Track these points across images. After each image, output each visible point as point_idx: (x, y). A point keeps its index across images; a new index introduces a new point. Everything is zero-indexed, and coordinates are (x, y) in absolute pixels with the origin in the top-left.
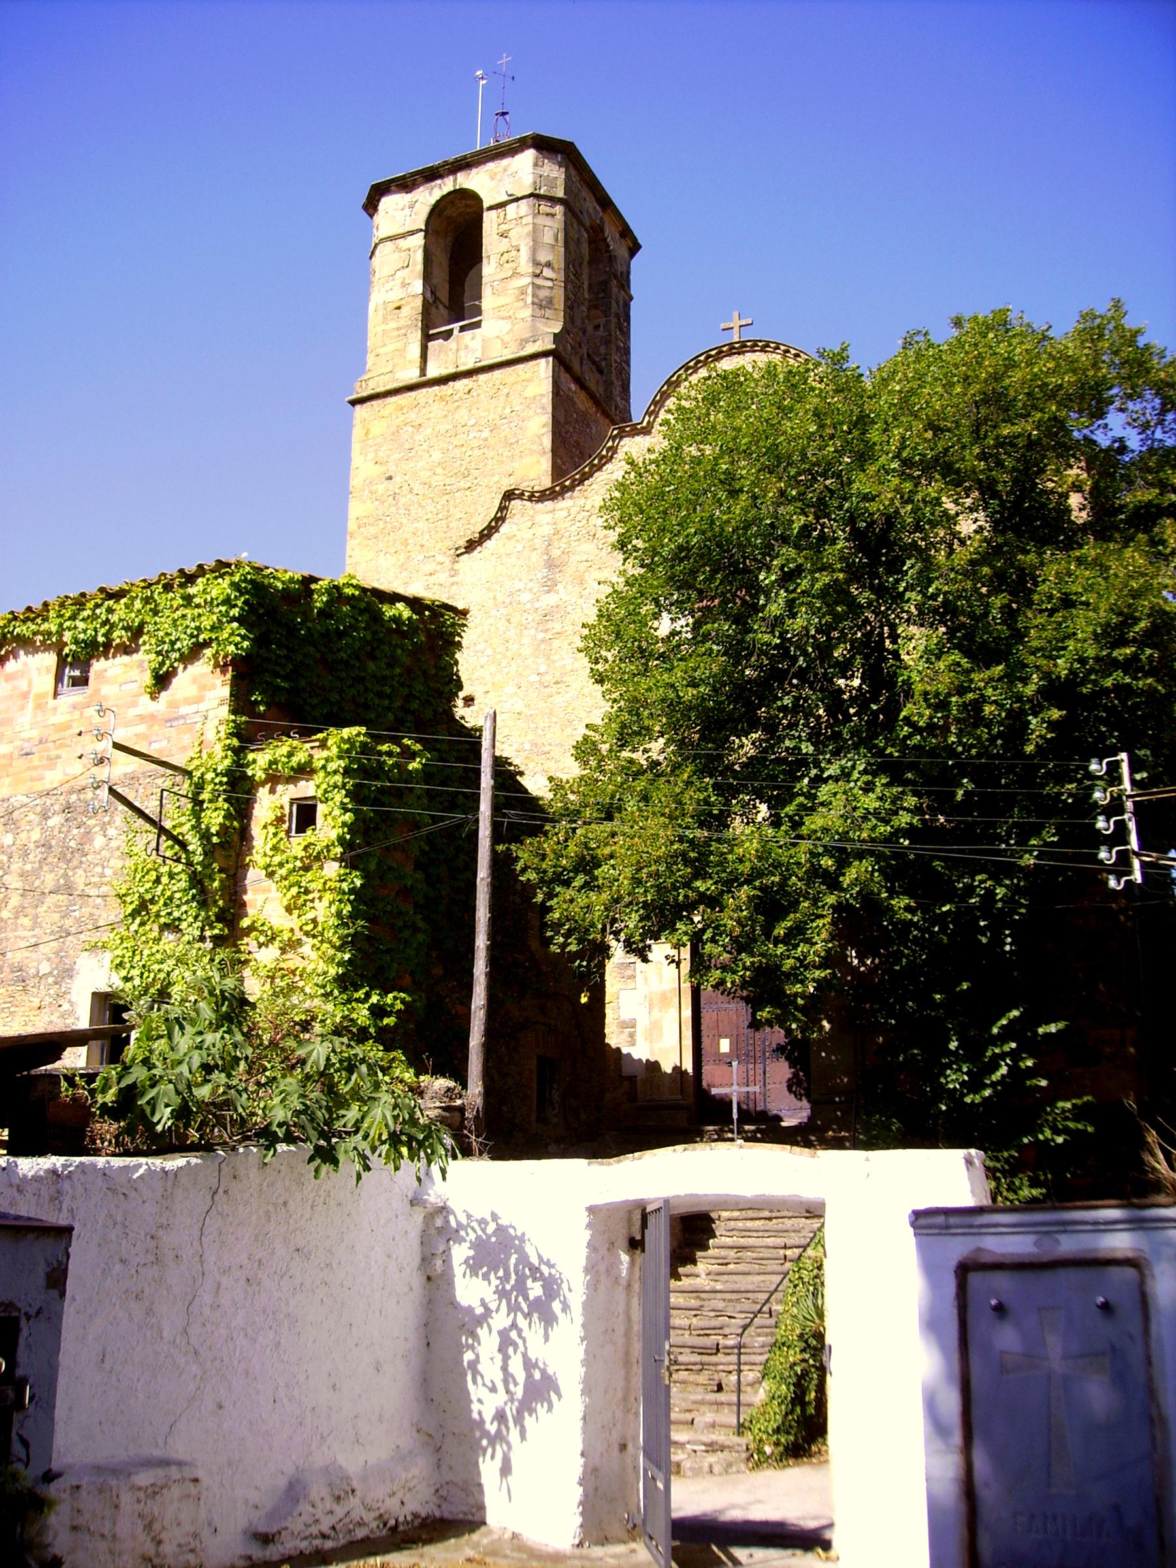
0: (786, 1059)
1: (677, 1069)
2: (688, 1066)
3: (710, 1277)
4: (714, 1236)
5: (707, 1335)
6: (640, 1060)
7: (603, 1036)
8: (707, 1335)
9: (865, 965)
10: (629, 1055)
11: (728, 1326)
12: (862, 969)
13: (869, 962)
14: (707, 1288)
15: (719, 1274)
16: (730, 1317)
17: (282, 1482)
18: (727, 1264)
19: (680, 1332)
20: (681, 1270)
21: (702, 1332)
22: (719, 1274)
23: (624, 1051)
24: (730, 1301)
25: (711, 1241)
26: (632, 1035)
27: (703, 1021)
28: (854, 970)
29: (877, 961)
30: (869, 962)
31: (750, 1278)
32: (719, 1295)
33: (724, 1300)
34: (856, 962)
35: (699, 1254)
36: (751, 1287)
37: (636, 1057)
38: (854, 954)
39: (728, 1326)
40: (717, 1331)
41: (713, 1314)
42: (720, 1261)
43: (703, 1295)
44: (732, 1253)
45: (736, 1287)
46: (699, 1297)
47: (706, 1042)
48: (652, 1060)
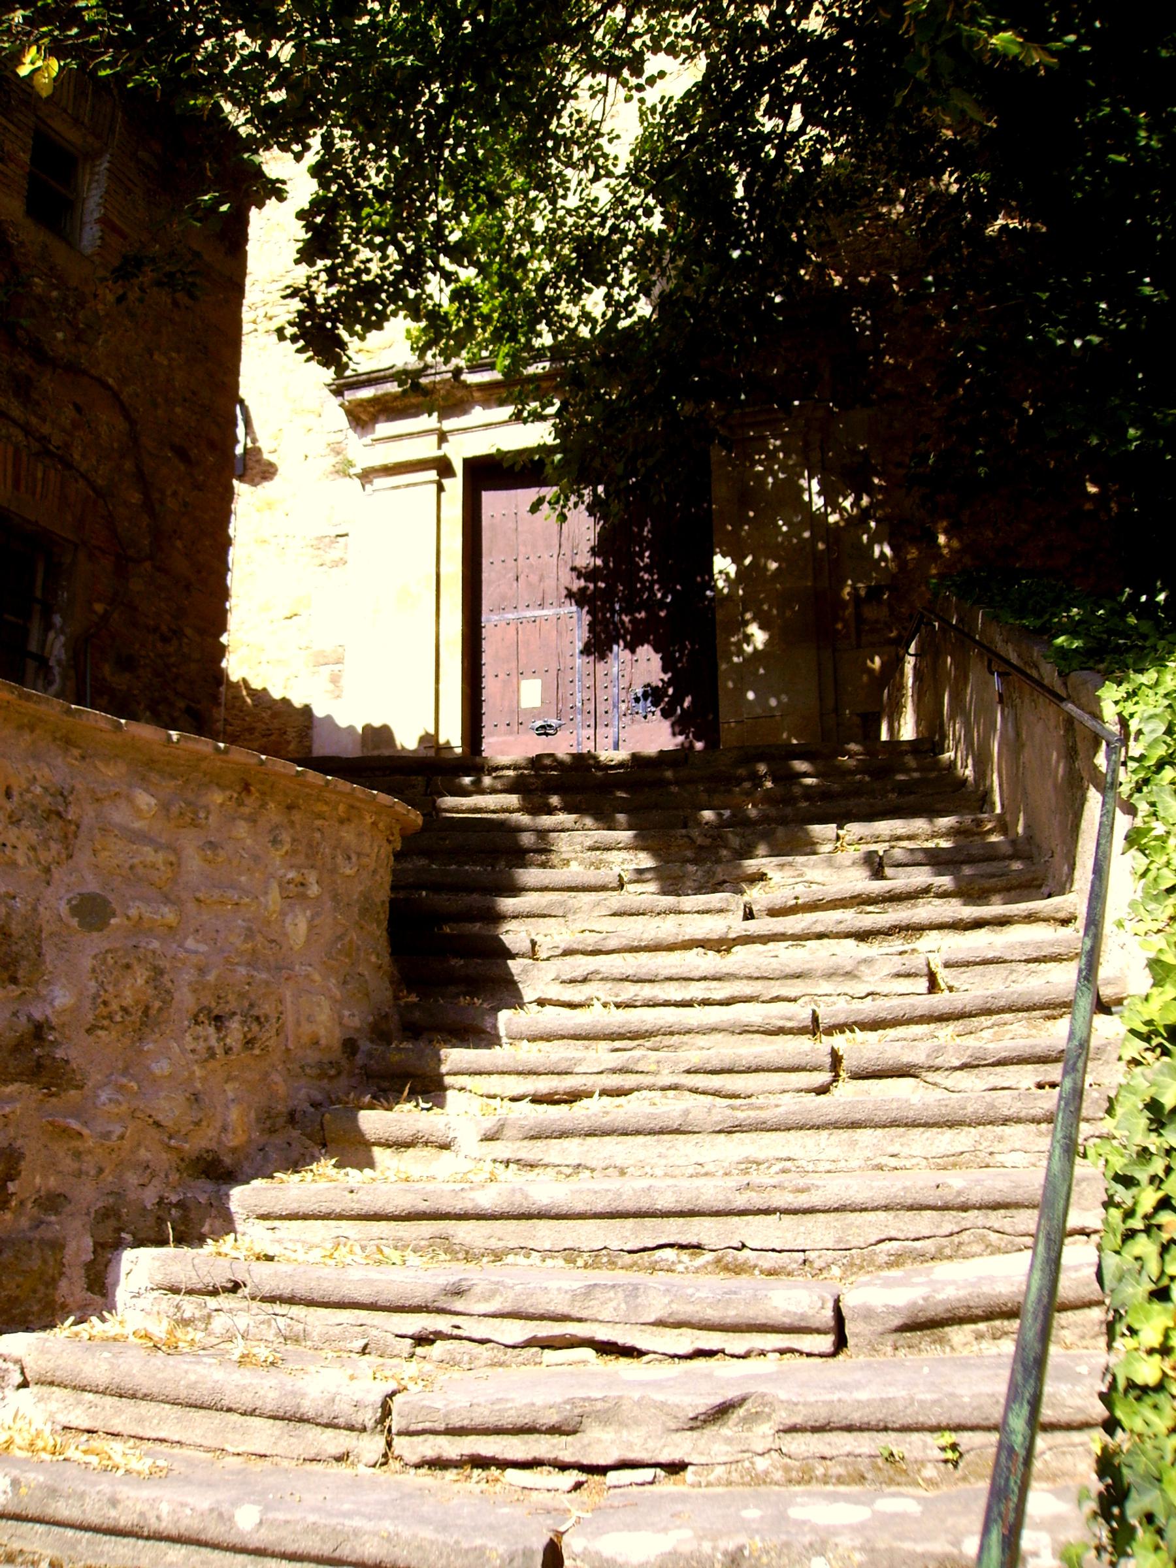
0: (666, 714)
1: (429, 740)
2: (452, 734)
3: (501, 1149)
4: (515, 1000)
5: (480, 1462)
6: (351, 729)
7: (227, 527)
8: (480, 1462)
9: (837, 508)
10: (329, 719)
11: (609, 1415)
12: (833, 518)
13: (847, 504)
14: (486, 1200)
15: (537, 1135)
16: (607, 1348)
17: (327, 1396)
18: (573, 1097)
19: (333, 1442)
20: (372, 1121)
21: (453, 1448)
22: (537, 1135)
23: (319, 712)
24: (599, 1257)
25: (504, 1016)
26: (335, 680)
27: (485, 645)
28: (816, 521)
29: (865, 501)
30: (847, 504)
31: (683, 1149)
32: (546, 1233)
33: (570, 1254)
34: (818, 502)
35: (454, 1057)
36: (710, 1193)
37: (342, 722)
38: (815, 487)
39: (609, 1415)
40: (540, 1447)
41: (517, 1331)
42: (544, 1085)
43: (464, 1232)
44: (602, 1055)
45: (629, 1193)
46: (445, 1244)
47: (491, 687)
48: (377, 724)
